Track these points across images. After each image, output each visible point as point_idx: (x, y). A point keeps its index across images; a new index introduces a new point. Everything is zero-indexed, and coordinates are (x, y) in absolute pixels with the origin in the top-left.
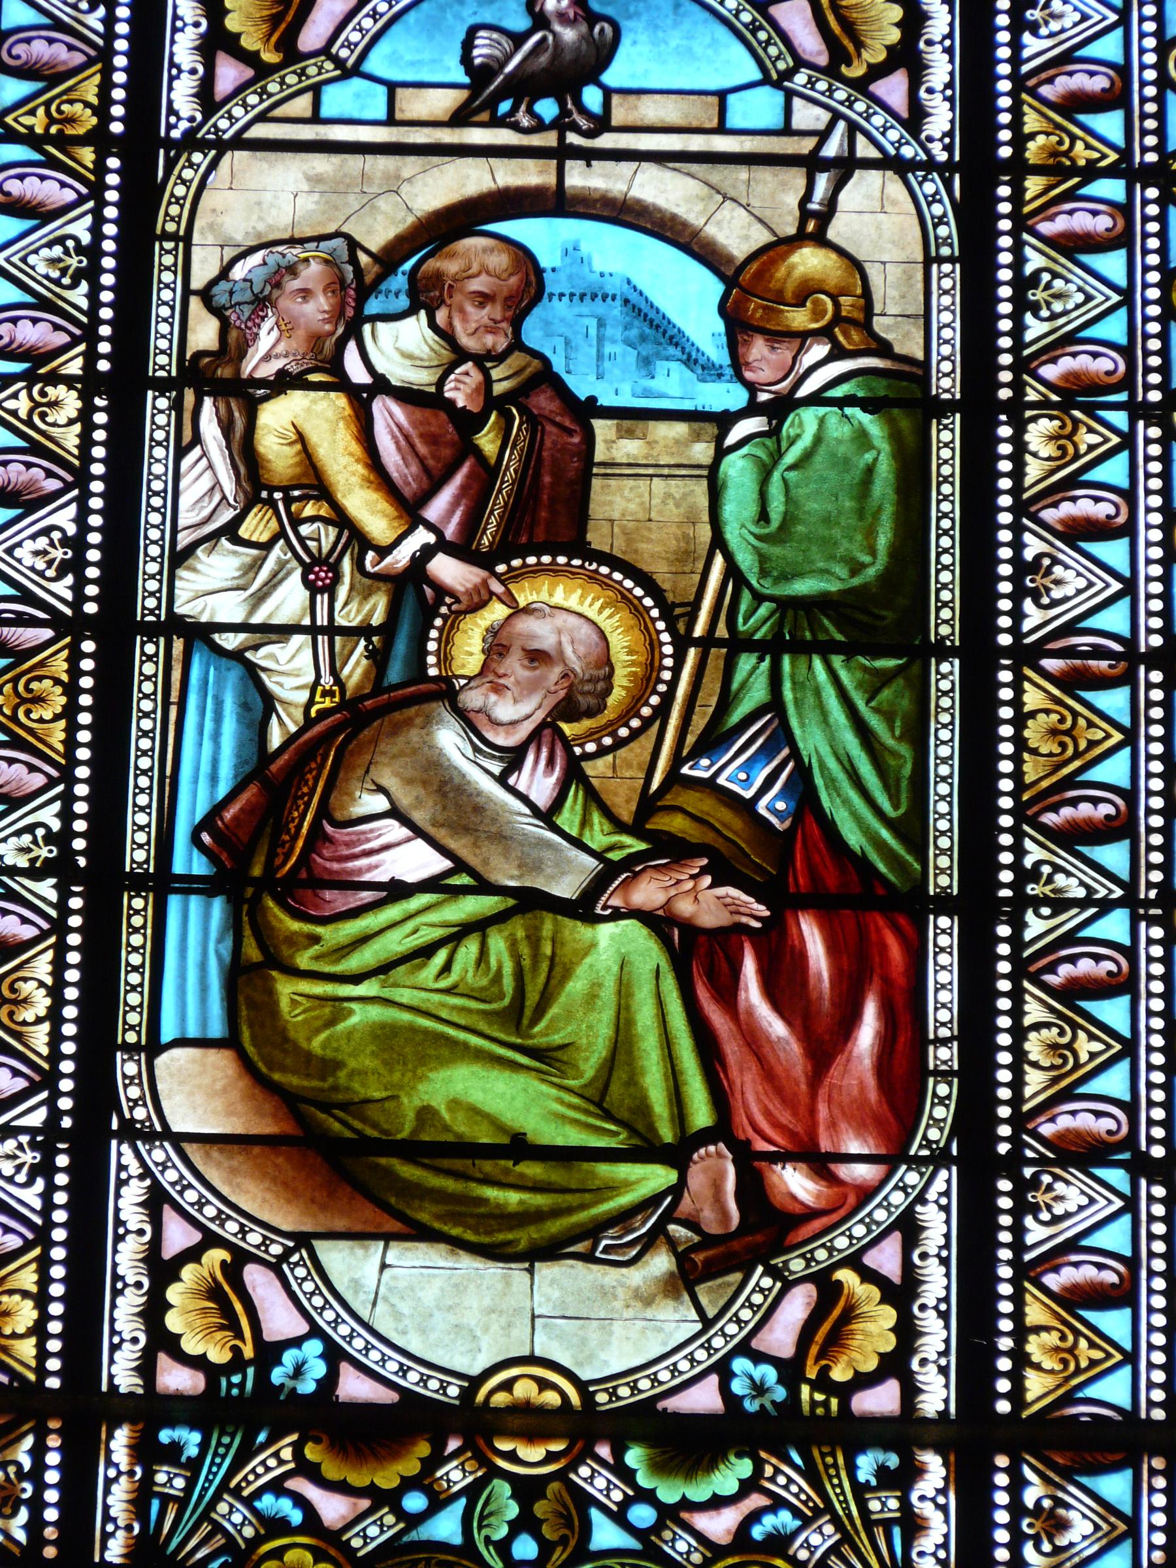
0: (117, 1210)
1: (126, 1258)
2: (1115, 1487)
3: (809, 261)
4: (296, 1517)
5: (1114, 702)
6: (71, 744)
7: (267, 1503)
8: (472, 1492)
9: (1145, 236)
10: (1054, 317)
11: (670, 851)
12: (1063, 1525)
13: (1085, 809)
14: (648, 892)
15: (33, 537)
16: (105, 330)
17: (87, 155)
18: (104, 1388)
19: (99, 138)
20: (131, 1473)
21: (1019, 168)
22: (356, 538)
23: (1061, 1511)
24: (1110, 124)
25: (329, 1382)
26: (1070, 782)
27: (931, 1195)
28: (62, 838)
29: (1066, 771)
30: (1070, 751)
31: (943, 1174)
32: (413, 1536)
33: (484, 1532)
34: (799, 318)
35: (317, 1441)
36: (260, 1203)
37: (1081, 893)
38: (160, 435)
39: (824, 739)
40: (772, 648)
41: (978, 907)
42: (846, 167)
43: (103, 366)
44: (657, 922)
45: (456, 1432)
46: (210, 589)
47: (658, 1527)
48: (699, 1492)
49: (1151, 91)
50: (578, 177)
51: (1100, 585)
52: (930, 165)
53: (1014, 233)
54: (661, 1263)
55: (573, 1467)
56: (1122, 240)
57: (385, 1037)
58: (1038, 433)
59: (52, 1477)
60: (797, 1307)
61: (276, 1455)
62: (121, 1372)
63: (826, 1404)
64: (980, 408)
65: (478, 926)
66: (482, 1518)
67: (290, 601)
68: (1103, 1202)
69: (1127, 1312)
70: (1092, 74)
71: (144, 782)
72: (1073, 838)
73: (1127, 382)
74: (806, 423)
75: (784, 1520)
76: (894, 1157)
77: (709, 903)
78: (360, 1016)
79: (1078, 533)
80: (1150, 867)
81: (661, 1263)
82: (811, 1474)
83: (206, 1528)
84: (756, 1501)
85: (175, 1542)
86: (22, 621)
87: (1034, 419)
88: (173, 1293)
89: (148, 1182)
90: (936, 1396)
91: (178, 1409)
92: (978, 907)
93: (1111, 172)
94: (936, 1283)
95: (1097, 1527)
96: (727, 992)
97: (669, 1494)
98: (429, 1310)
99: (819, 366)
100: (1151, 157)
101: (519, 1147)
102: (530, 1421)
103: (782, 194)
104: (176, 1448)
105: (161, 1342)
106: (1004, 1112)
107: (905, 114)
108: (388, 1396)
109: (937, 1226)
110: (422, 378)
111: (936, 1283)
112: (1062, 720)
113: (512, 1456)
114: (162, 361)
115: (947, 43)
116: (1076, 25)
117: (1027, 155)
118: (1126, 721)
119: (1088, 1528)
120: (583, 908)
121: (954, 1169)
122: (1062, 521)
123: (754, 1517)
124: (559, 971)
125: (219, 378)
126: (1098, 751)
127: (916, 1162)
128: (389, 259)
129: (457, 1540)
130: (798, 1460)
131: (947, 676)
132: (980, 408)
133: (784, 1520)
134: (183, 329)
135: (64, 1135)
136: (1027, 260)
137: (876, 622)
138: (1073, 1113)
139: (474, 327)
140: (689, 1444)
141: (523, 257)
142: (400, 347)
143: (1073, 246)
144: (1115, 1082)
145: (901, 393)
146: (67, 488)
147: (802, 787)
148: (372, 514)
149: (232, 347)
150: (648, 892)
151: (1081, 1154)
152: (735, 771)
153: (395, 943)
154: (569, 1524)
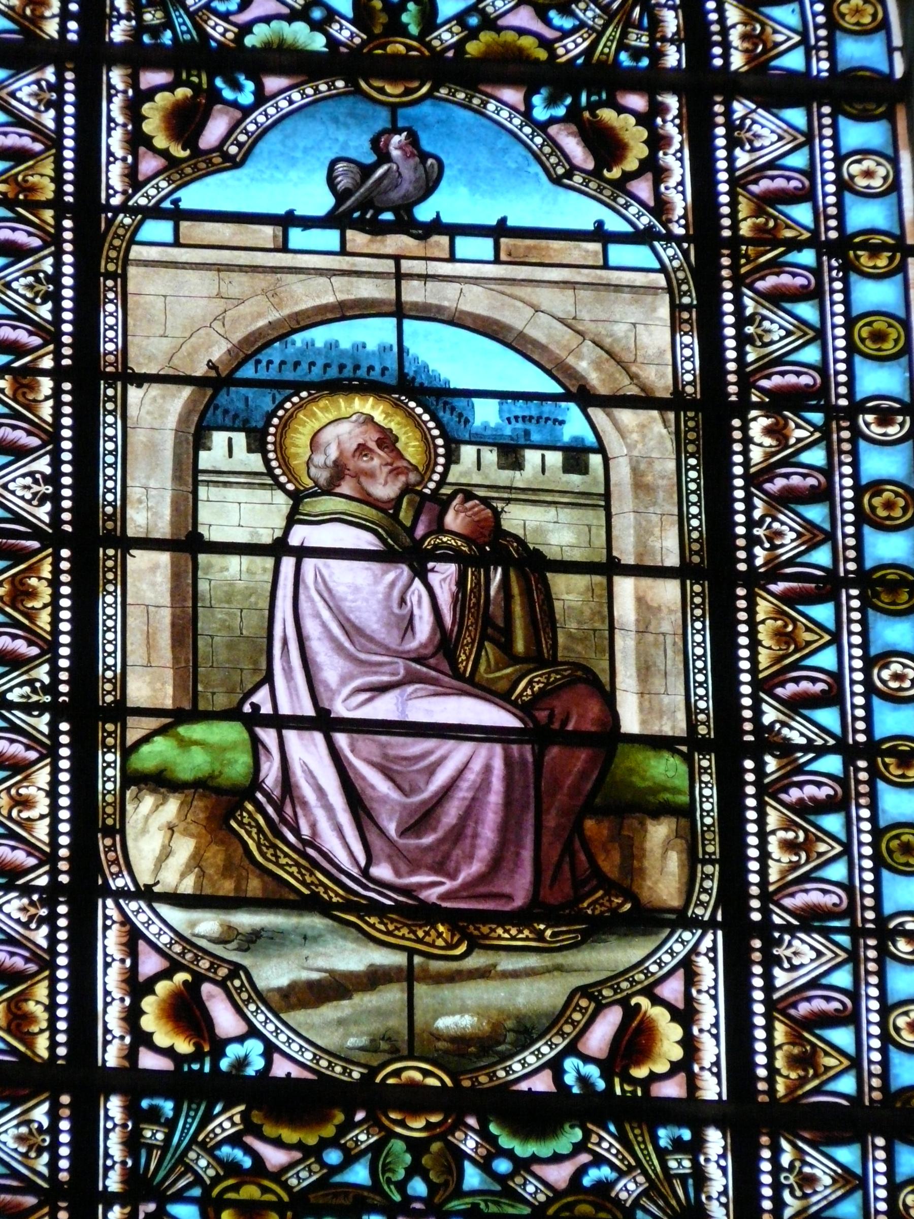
1: (110, 980)
2: (847, 1155)
4: (247, 1162)
5: (823, 613)
8: (376, 1149)
9: (824, 172)
13: (805, 685)
15: (24, 476)
17: (48, 215)
18: (101, 1188)
19: (57, 203)
20: (125, 1126)
25: (269, 1063)
27: (703, 948)
28: (51, 689)
30: (13, 791)
31: (710, 936)
33: (388, 1175)
35: (260, 1109)
37: (803, 741)
43: (62, 1051)
45: (362, 1107)
47: (511, 1176)
48: (544, 1150)
49: (822, 33)
56: (814, 294)
58: (758, 425)
62: (112, 1057)
66: (384, 1165)
68: (830, 955)
70: (789, 179)
73: (850, 912)
75: (605, 1172)
79: (777, 298)
82: (622, 1138)
84: (585, 1158)
85: (162, 1174)
87: (755, 419)
88: (149, 1004)
89: (128, 928)
90: (711, 1089)
91: (155, 1083)
94: (114, 141)
97: (523, 1150)
100: (833, 235)
106: (754, 891)
107: (652, 203)
112: (786, 626)
115: (109, 1037)
116: (782, 338)
117: (742, 232)
118: (842, 836)
121: (720, 933)
123: (582, 1171)
126: (832, 1073)
130: (612, 1128)
133: (605, 1172)
146: (47, 149)
151: (811, 920)
154: (450, 1172)
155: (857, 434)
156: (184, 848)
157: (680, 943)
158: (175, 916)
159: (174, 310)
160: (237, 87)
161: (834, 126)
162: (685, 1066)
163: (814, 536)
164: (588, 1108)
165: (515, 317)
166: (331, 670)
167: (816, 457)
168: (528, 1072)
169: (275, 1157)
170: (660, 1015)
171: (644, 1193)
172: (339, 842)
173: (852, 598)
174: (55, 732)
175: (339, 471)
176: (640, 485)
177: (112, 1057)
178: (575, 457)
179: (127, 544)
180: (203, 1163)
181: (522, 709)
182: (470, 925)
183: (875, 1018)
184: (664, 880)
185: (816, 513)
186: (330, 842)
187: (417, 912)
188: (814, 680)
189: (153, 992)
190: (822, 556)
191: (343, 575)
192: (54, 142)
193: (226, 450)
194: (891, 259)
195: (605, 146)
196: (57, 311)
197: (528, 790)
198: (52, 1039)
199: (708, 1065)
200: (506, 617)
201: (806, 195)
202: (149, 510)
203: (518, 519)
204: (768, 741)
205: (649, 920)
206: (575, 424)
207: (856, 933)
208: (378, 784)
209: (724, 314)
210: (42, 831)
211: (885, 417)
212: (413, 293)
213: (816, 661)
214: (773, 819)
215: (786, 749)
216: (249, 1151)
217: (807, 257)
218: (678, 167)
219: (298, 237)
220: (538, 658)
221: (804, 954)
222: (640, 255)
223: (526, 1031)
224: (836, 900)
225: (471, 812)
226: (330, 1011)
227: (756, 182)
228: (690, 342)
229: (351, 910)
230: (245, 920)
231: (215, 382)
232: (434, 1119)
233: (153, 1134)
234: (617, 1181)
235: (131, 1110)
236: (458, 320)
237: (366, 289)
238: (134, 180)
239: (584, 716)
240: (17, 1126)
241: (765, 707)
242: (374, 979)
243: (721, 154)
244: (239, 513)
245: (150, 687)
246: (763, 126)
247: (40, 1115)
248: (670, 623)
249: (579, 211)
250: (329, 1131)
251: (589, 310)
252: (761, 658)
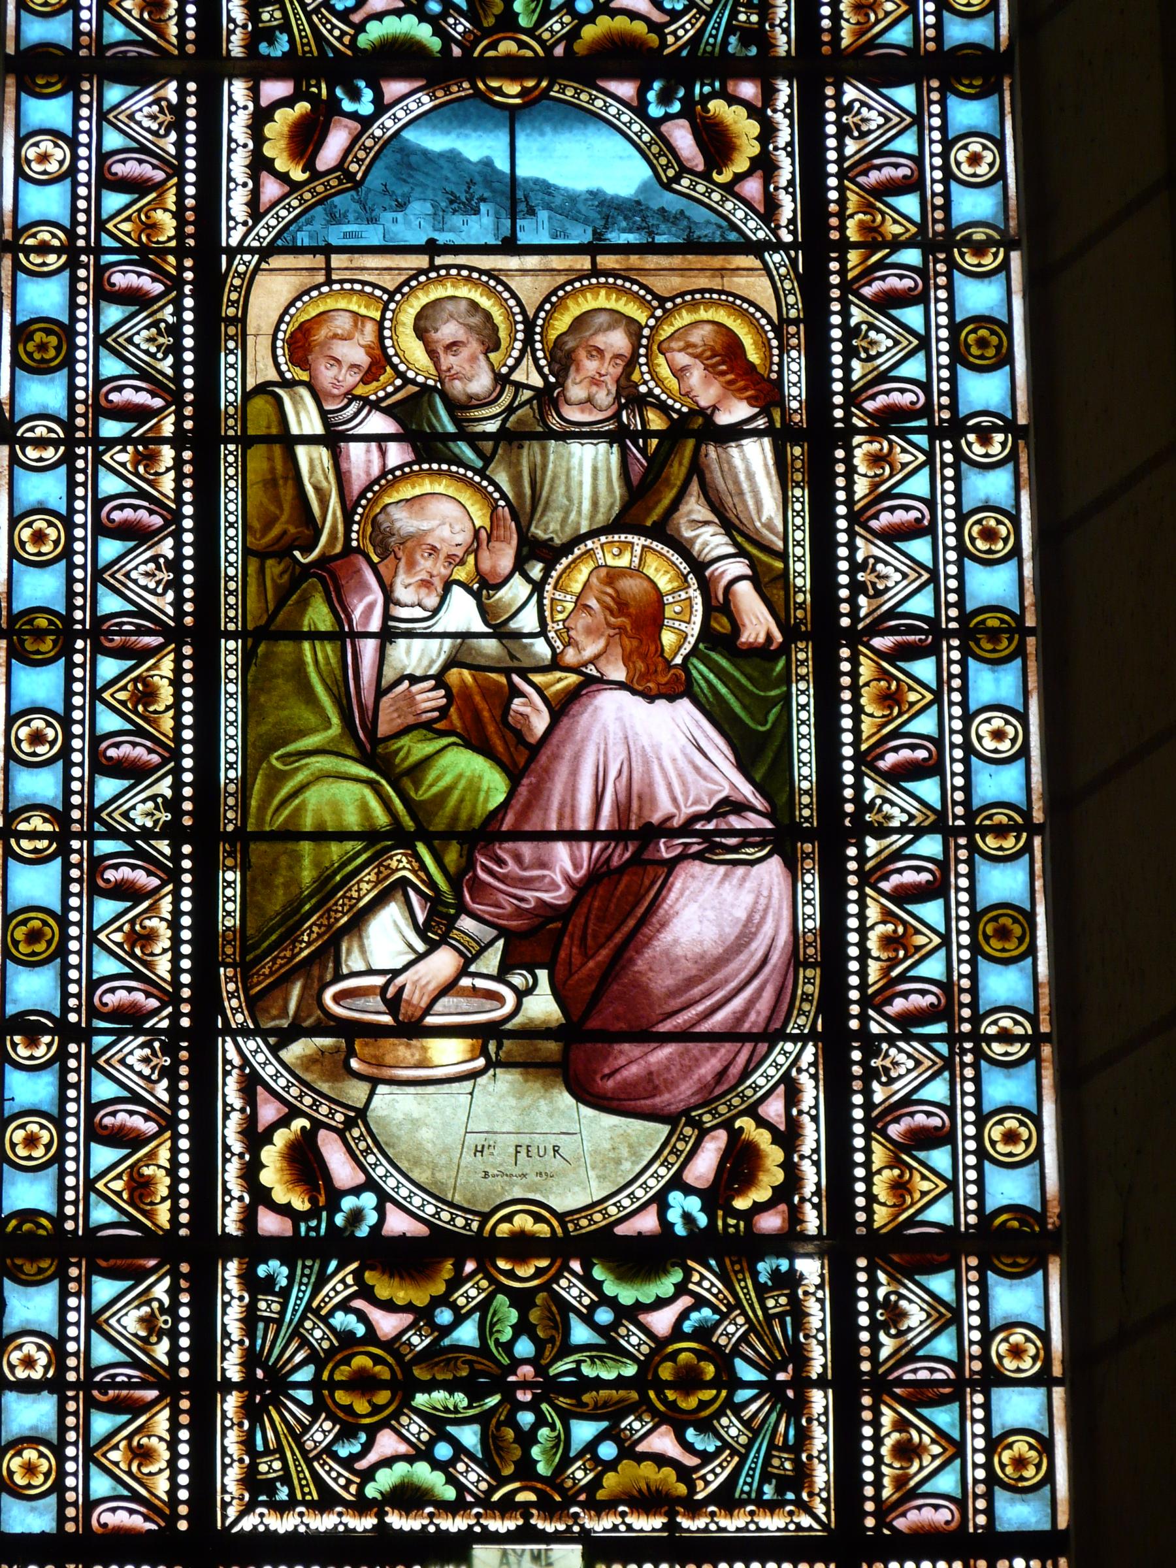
0: (229, 171)
1: (230, 1131)
2: (942, 1284)
5: (924, 669)
6: (178, 727)
7: (341, 1320)
8: (484, 1307)
10: (870, 359)
12: (904, 1315)
15: (144, 801)
16: (187, 806)
17: (164, 846)
19: (181, 252)
23: (903, 1303)
24: (909, 204)
25: (642, 93)
26: (895, 734)
27: (804, 1064)
28: (173, 804)
29: (883, 488)
32: (447, 1342)
35: (372, 1269)
38: (231, 572)
47: (615, 1325)
51: (896, 120)
52: (779, 246)
53: (859, 888)
55: (556, 1278)
56: (920, 298)
59: (184, 1312)
61: (343, 1281)
62: (230, 1222)
63: (736, 1226)
69: (937, 779)
70: (936, 1507)
71: (232, 600)
72: (894, 536)
79: (887, 302)
80: (948, 605)
83: (756, 1424)
84: (362, 1465)
86: (140, 631)
88: (269, 130)
91: (745, 69)
93: (910, 244)
95: (929, 1315)
97: (627, 1295)
104: (271, 1279)
108: (421, 1230)
109: (810, 1093)
111: (237, 165)
113: (511, 1275)
119: (923, 1316)
122: (878, 410)
127: (794, 1039)
129: (477, 1344)
135: (185, 1383)
136: (881, 1345)
138: (919, 1508)
146: (164, 884)
154: (495, 1438)
155: (951, 264)
160: (355, 96)
161: (982, 1284)
167: (919, 485)
170: (763, 1138)
171: (306, 1429)
174: (177, 856)
177: (230, 1222)
180: (318, 1334)
183: (971, 1130)
188: (923, 993)
189: (271, 1142)
194: (1018, 839)
196: (178, 365)
198: (172, 1479)
199: (807, 1152)
201: (913, 184)
209: (841, 660)
210: (163, 966)
213: (924, 970)
214: (873, 913)
216: (362, 1317)
217: (912, 256)
224: (911, 283)
227: (865, 173)
232: (530, 84)
233: (267, 1306)
234: (718, 1324)
235: (249, 1280)
240: (138, 1307)
241: (849, 194)
243: (831, 143)
246: (910, 1301)
250: (440, 1288)
252: (864, 727)
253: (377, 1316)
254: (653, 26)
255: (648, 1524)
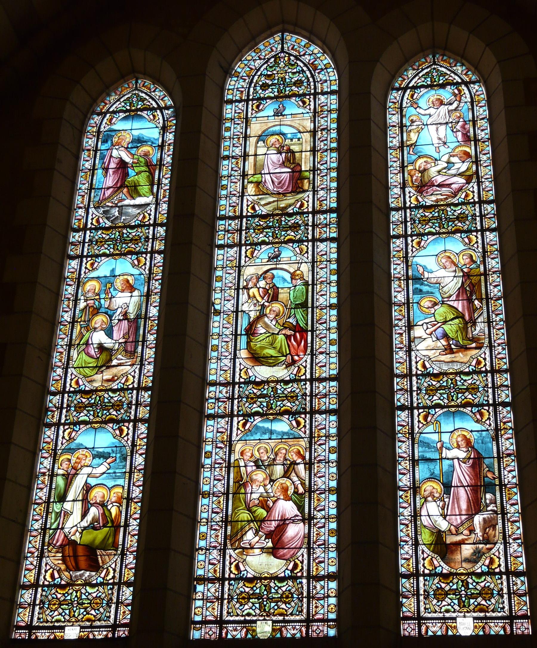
1: (227, 563)
3: (298, 272)
11: (286, 328)
14: (284, 332)
21: (317, 262)
22: (258, 301)
28: (222, 517)
34: (297, 278)
36: (249, 364)
39: (299, 316)
40: (294, 308)
41: (312, 331)
42: (301, 263)
44: (284, 335)
46: (245, 308)
50: (278, 266)
54: (284, 366)
56: (327, 117)
57: (260, 347)
58: (320, 132)
60: (296, 369)
62: (308, 416)
64: (313, 284)
65: (269, 336)
67: (252, 308)
74: (297, 287)
76: (305, 355)
77: (289, 332)
78: (258, 345)
79: (322, 118)
81: (284, 366)
92: (312, 331)
96: (290, 341)
97: (279, 585)
98: (263, 372)
99: (299, 282)
101: (272, 356)
102: (273, 382)
103: (296, 266)
105: (241, 377)
109: (309, 361)
110: (264, 286)
114: (241, 287)
120: (278, 334)
124: (276, 340)
125: (246, 288)
128: (261, 275)
131: (310, 310)
132: (313, 284)
134: (242, 284)
137: (304, 305)
139: (269, 281)
140: (286, 383)
141: (273, 274)
142: (262, 284)
143: (321, 268)
144: (324, 346)
145: (306, 284)
147: (297, 321)
148: (259, 299)
149: (247, 285)
150: (284, 332)
151: (321, 353)
152: (291, 320)
153: (261, 338)
156: (254, 189)
157: (307, 193)
158: (252, 197)
159: (255, 129)
162: (473, 198)
163: (325, 145)
164: (297, 213)
165: (293, 124)
166: (270, 167)
167: (326, 136)
168: (290, 210)
169: (262, 223)
172: (270, 186)
173: (327, 493)
175: (273, 144)
176: (306, 142)
178: (299, 139)
179: (248, 156)
181: (292, 169)
182: (284, 194)
184: (306, 186)
185: (325, 142)
186: (270, 187)
187: (279, 194)
190: (326, 147)
191: (272, 156)
192: (243, 111)
193: (261, 143)
195: (304, 103)
197: (292, 178)
200: (290, 159)
202: (252, 152)
203: (292, 147)
204: (319, 169)
205: (304, 191)
206: (299, 135)
207: (325, 548)
208: (275, 179)
211: (333, 437)
212: (282, 123)
214: (315, 530)
215: (320, 170)
218: (312, 104)
219: (270, 118)
220: (293, 163)
221: (321, 193)
222: (307, 115)
223: (290, 206)
225: (285, 182)
226: (269, 206)
228: (312, 124)
229: (272, 194)
230: (260, 197)
231: (260, 136)
233: (249, 222)
236: (287, 125)
237: (277, 123)
238: (252, 114)
239: (298, 169)
242: (274, 202)
244: (261, 151)
245: (251, 172)
247: (412, 581)
248: (308, 157)
249: (301, 110)
251: (301, 122)
253: (246, 589)
254: (473, 400)
255: (281, 618)
